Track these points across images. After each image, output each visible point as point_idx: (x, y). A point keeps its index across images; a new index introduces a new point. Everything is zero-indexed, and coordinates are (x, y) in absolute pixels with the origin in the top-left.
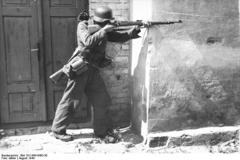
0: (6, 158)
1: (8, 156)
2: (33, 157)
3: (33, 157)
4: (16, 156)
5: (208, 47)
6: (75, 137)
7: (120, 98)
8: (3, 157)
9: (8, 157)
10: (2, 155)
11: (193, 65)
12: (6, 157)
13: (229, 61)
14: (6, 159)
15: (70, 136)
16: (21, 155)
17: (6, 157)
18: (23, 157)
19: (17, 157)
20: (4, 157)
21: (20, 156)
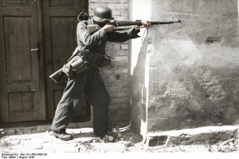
0: (6, 157)
1: (8, 155)
3: (33, 156)
4: (16, 155)
5: (207, 46)
6: (75, 136)
8: (3, 156)
9: (8, 156)
10: (2, 154)
12: (6, 156)
15: (70, 136)
16: (21, 155)
17: (6, 156)
18: (23, 156)
19: (17, 156)
20: (4, 156)
21: (20, 155)
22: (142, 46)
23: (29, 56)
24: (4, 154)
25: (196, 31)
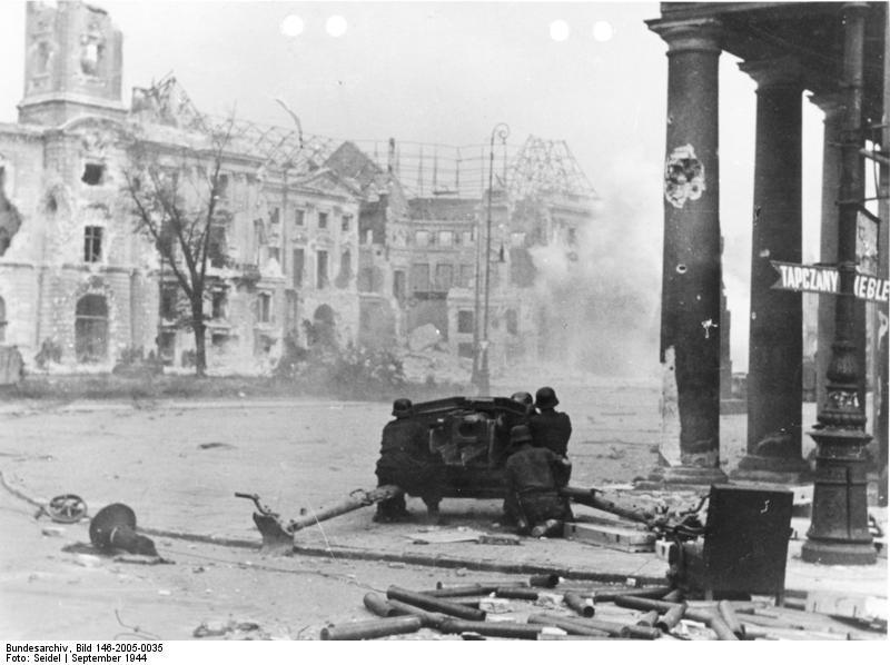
0: (24, 659)
1: (31, 648)
2: (142, 654)
3: (142, 654)
4: (60, 650)
5: (345, 406)
6: (851, 558)
7: (138, 202)
8: (12, 652)
9: (30, 655)
10: (9, 647)
11: (708, 211)
12: (22, 654)
13: (535, 605)
14: (92, 663)
15: (548, 575)
16: (79, 648)
17: (22, 654)
18: (86, 654)
19: (63, 654)
20: (16, 654)
21: (74, 651)
22: (558, 409)
23: (10, 269)
24: (14, 644)
25: (445, 377)
